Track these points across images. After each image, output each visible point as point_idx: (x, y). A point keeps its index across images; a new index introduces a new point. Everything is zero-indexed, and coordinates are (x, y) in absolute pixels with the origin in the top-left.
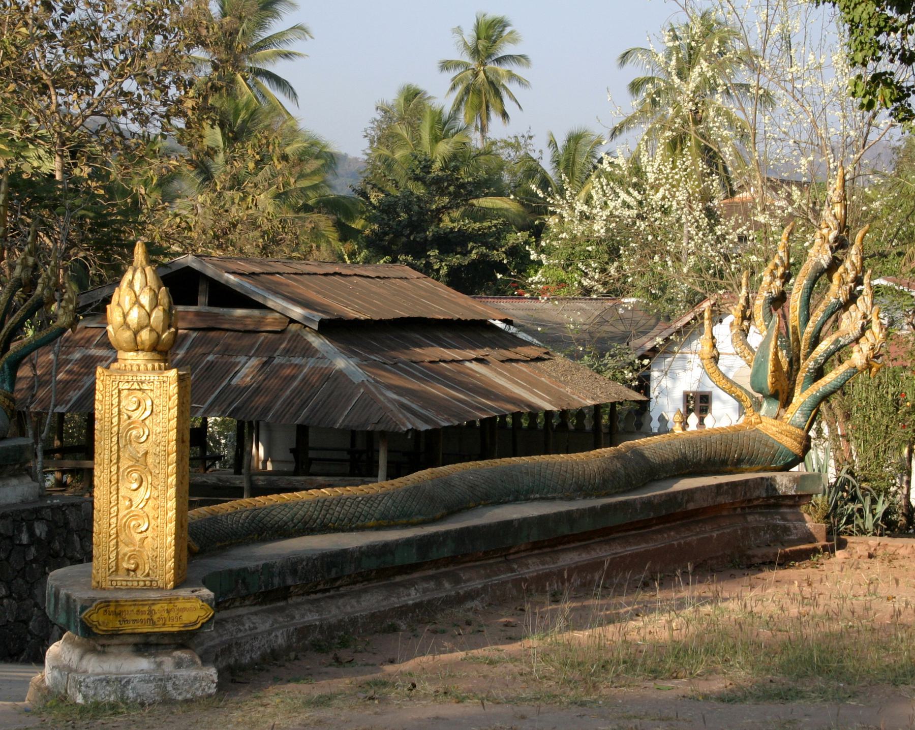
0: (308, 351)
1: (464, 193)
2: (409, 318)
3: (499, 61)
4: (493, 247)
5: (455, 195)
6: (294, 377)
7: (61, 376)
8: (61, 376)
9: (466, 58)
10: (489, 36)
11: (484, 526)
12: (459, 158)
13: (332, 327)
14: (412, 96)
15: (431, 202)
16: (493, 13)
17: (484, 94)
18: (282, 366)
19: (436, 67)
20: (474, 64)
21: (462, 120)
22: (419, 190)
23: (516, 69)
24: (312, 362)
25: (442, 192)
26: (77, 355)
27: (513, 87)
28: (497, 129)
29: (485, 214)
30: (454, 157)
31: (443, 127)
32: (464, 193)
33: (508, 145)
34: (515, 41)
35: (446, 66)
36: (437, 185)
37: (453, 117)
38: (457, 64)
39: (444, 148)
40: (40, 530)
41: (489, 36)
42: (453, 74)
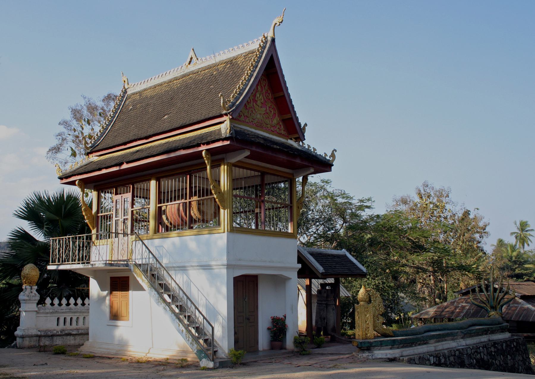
0: (518, 303)
1: (521, 264)
2: (531, 296)
3: (527, 231)
4: (530, 277)
5: (519, 265)
6: (516, 310)
7: (457, 310)
8: (457, 310)
9: (517, 231)
10: (523, 226)
11: (260, 375)
12: (519, 255)
13: (524, 297)
14: (501, 241)
15: (513, 266)
16: (524, 220)
17: (523, 240)
18: (512, 307)
19: (509, 234)
20: (519, 232)
21: (518, 246)
22: (510, 264)
23: (531, 233)
24: (520, 306)
25: (516, 264)
26: (460, 305)
27: (530, 238)
28: (526, 248)
29: (527, 269)
30: (518, 255)
31: (513, 248)
32: (521, 264)
33: (529, 251)
34: (529, 227)
35: (512, 234)
36: (515, 262)
37: (515, 245)
38: (515, 233)
39: (515, 254)
40: (515, 344)
41: (523, 226)
42: (514, 235)
